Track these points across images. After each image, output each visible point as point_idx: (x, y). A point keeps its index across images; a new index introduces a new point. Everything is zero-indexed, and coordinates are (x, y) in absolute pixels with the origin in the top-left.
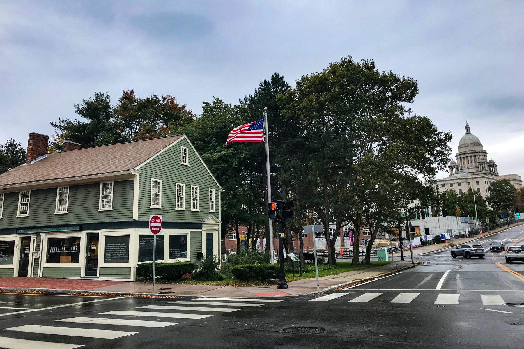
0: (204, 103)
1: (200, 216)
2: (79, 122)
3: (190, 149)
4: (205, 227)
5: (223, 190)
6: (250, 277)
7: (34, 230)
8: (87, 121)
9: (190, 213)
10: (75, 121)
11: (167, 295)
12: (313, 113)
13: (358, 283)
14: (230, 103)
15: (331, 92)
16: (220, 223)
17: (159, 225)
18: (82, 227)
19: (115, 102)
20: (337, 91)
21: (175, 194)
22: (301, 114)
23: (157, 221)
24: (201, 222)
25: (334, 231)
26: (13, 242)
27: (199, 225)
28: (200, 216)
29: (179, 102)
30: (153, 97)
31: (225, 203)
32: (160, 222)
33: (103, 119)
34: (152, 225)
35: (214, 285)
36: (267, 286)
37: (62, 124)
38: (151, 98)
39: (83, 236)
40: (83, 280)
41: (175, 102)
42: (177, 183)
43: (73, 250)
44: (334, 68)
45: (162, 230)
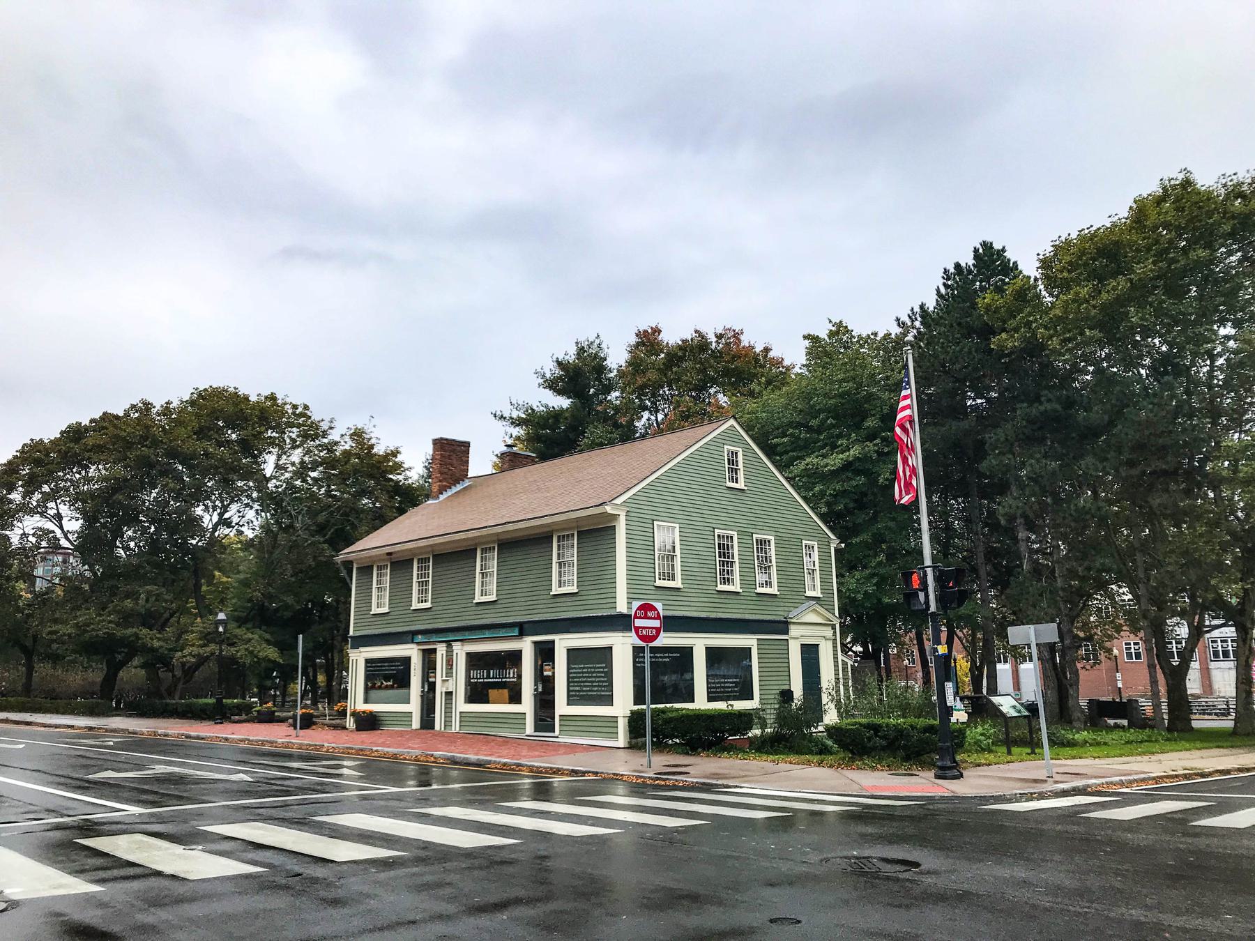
0: (805, 337)
1: (782, 604)
2: (547, 406)
3: (747, 449)
4: (794, 631)
5: (840, 543)
6: (874, 749)
7: (441, 635)
8: (564, 403)
9: (754, 599)
10: (539, 404)
11: (668, 779)
12: (1082, 334)
13: (1186, 777)
14: (875, 329)
15: (1134, 272)
16: (837, 622)
17: (656, 623)
18: (523, 629)
19: (617, 357)
20: (1151, 270)
21: (752, 558)
22: (1051, 337)
23: (649, 614)
24: (785, 618)
25: (1235, 644)
26: (407, 660)
27: (782, 627)
28: (782, 604)
29: (754, 339)
30: (694, 335)
31: (869, 574)
32: (658, 617)
33: (596, 394)
34: (639, 623)
35: (790, 763)
36: (914, 773)
37: (515, 414)
38: (692, 339)
39: (526, 645)
40: (529, 739)
41: (745, 341)
42: (716, 531)
43: (509, 678)
44: (1141, 210)
45: (662, 634)
